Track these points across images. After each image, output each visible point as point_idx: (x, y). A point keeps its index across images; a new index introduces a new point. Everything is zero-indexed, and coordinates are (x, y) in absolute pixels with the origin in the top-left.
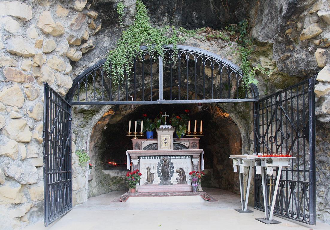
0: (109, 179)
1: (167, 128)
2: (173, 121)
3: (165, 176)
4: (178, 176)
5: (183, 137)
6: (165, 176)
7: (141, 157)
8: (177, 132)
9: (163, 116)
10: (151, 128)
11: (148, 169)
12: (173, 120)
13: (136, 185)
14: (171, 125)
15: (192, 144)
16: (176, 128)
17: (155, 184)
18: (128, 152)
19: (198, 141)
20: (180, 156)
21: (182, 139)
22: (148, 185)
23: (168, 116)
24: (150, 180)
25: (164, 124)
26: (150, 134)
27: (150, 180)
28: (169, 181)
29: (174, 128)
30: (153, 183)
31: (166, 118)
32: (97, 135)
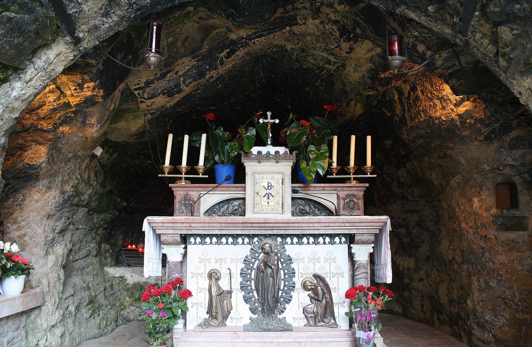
0: (122, 290)
1: (273, 152)
2: (291, 134)
3: (268, 300)
4: (308, 301)
5: (320, 179)
6: (268, 300)
7: (192, 239)
8: (303, 165)
9: (261, 121)
10: (229, 153)
11: (214, 276)
12: (292, 130)
13: (169, 330)
14: (287, 147)
15: (344, 199)
16: (299, 153)
17: (234, 324)
18: (149, 223)
19: (363, 193)
20: (316, 236)
21: (316, 185)
22: (210, 329)
23: (277, 121)
24: (218, 311)
25: (264, 144)
26: (224, 171)
27: (218, 311)
28: (280, 317)
29: (294, 153)
30: (228, 322)
31: (269, 126)
32: (73, 172)
